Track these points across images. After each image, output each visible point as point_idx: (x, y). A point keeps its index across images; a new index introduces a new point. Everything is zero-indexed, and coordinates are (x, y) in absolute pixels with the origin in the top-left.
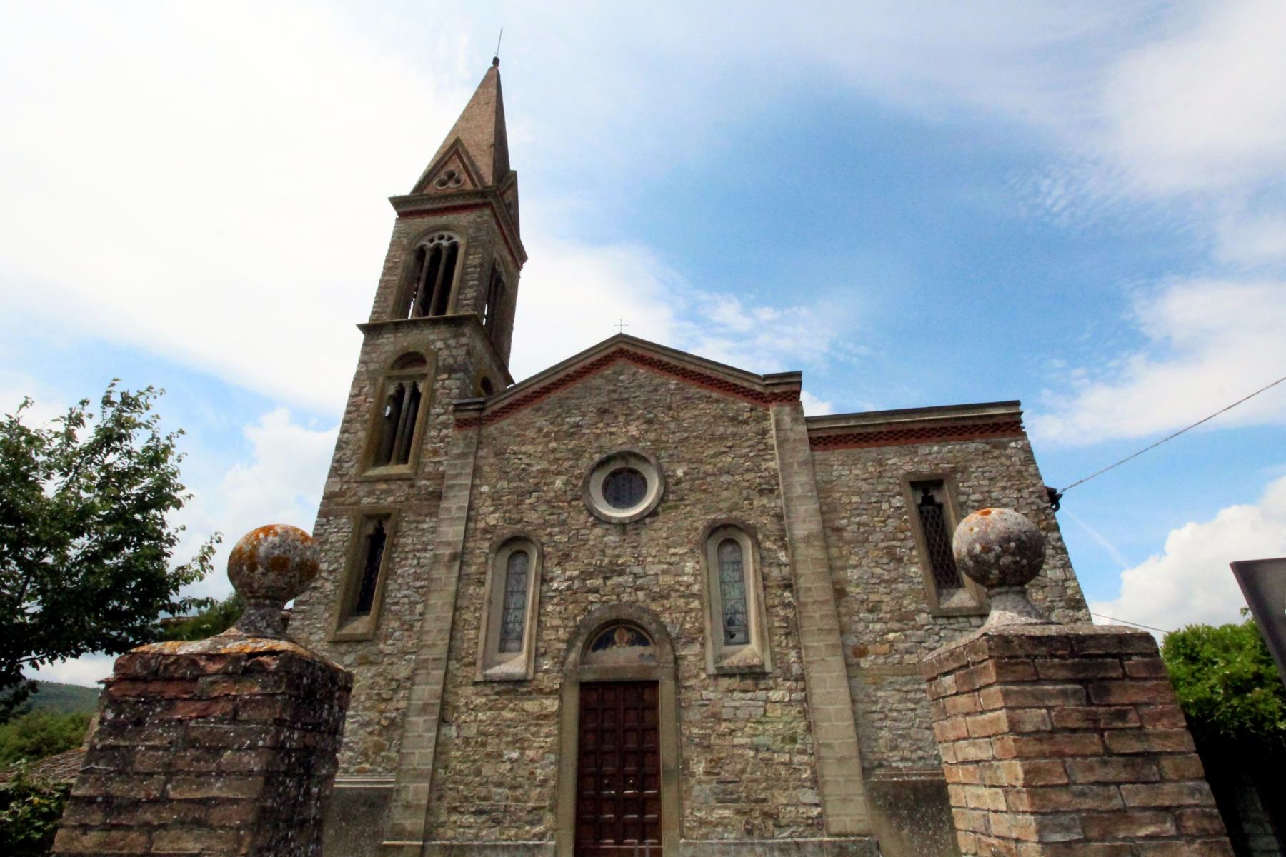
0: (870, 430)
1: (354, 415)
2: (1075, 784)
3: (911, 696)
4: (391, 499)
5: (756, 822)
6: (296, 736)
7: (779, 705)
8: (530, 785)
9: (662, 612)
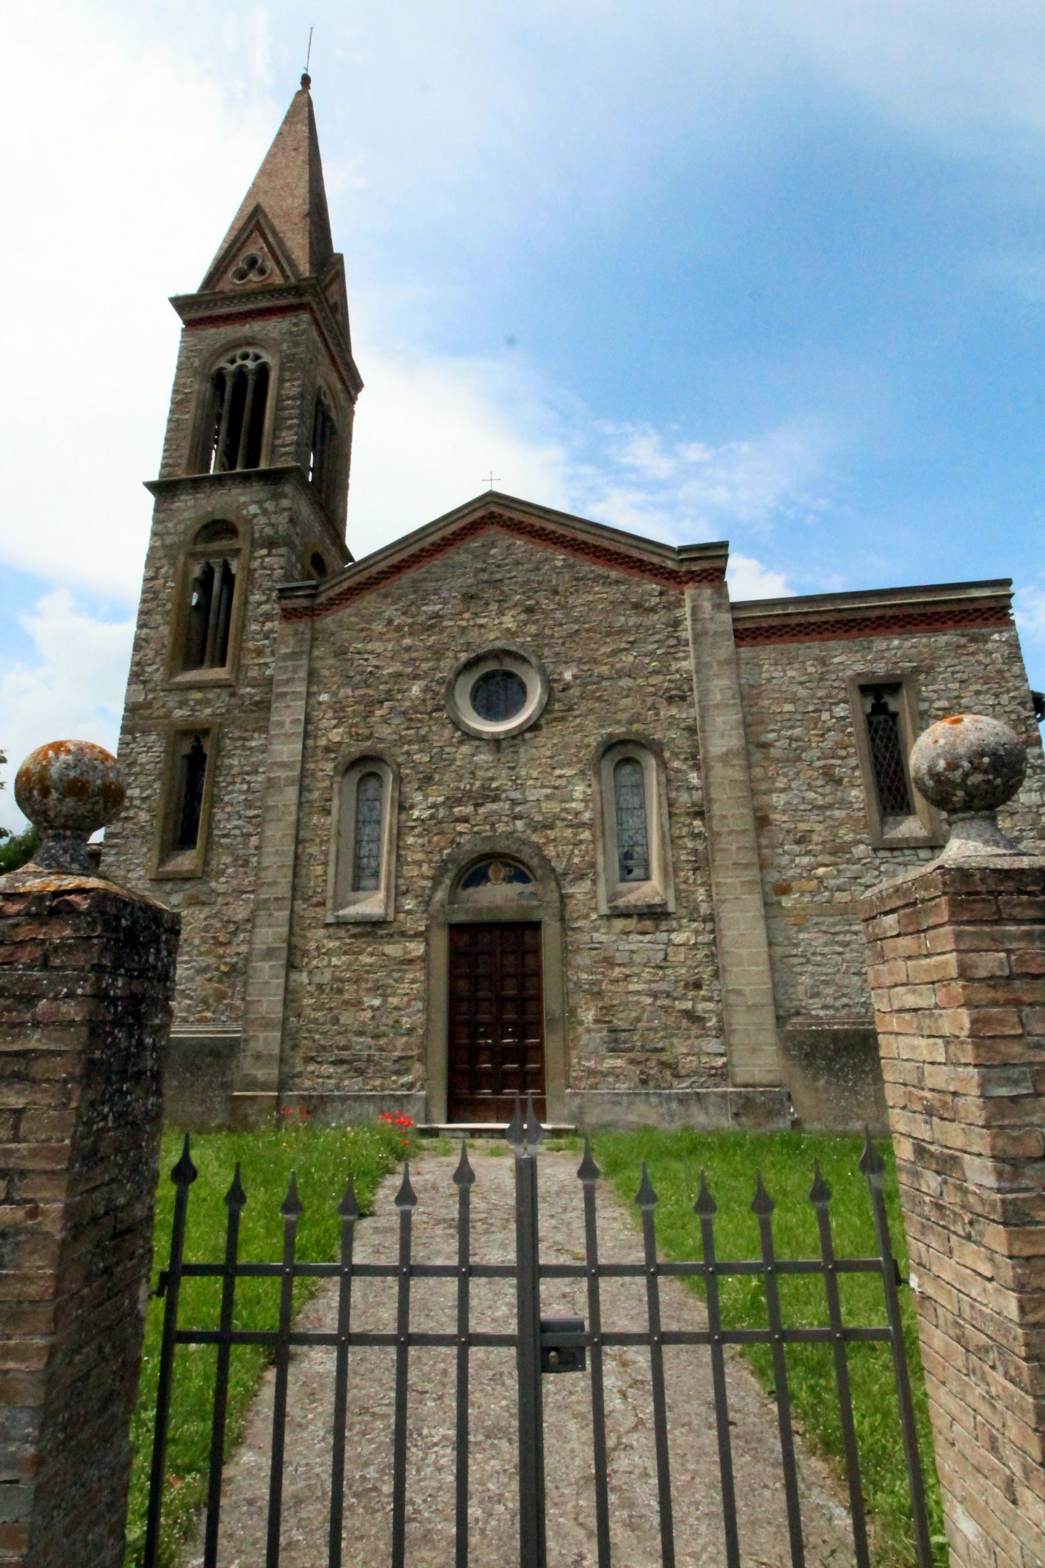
0: (812, 619)
1: (151, 605)
2: (1030, 1034)
3: (840, 938)
4: (208, 711)
5: (652, 1072)
6: (120, 983)
7: (682, 949)
8: (396, 1034)
9: (545, 844)
